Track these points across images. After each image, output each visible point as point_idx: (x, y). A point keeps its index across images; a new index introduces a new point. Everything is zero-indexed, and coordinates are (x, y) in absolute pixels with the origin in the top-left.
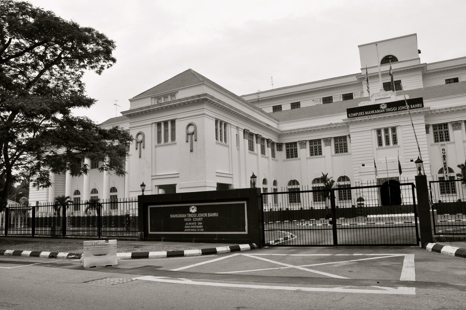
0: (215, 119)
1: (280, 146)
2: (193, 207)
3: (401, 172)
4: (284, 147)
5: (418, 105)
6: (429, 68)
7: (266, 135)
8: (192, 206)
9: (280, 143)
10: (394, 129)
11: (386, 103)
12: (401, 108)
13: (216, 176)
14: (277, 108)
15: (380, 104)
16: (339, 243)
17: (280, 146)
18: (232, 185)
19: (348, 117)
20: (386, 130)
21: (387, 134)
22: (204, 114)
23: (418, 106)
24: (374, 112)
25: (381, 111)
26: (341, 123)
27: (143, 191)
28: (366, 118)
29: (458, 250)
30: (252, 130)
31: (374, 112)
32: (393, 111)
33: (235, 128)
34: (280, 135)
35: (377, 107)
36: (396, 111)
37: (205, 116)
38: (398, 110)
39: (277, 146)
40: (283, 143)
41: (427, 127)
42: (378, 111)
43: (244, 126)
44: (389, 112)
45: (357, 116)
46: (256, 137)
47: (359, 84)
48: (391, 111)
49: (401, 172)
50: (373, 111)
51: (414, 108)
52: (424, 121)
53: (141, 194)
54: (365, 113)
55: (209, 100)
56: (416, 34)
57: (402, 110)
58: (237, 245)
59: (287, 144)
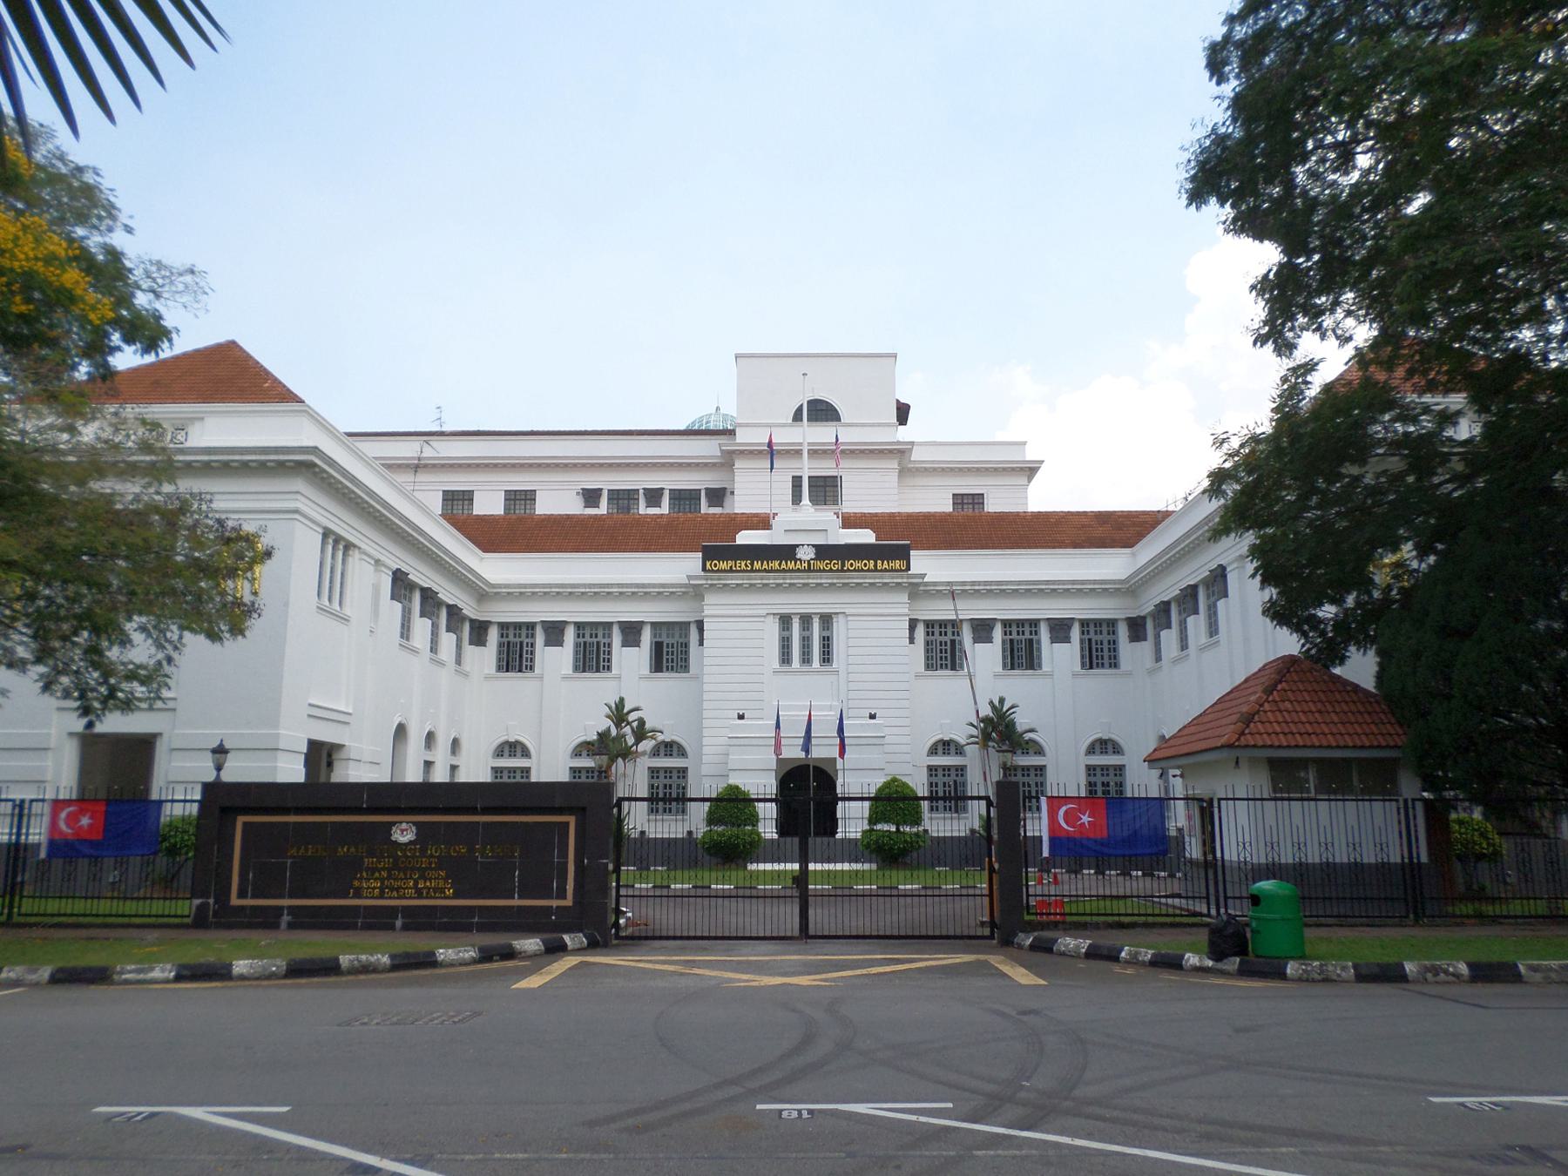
0: (321, 531)
1: (479, 632)
2: (404, 826)
3: (842, 753)
4: (493, 635)
5: (897, 564)
6: (917, 455)
7: (448, 593)
8: (401, 823)
9: (481, 619)
10: (827, 620)
11: (813, 546)
12: (852, 565)
13: (309, 716)
14: (458, 500)
15: (798, 546)
16: (811, 932)
17: (479, 632)
18: (345, 749)
19: (704, 569)
20: (806, 620)
21: (806, 633)
22: (296, 511)
23: (897, 565)
24: (780, 565)
25: (798, 566)
26: (681, 585)
27: (219, 768)
28: (757, 580)
29: (1090, 945)
30: (416, 573)
31: (780, 565)
32: (831, 570)
33: (373, 562)
34: (483, 593)
35: (787, 552)
36: (838, 571)
37: (297, 516)
38: (842, 570)
39: (472, 628)
40: (490, 622)
41: (913, 624)
42: (791, 565)
43: (398, 558)
44: (820, 571)
45: (731, 570)
46: (422, 596)
47: (722, 465)
48: (824, 571)
49: (842, 753)
50: (777, 563)
51: (886, 570)
52: (907, 610)
53: (210, 777)
54: (752, 564)
55: (317, 470)
56: (895, 356)
57: (855, 570)
58: (555, 935)
59: (503, 626)
